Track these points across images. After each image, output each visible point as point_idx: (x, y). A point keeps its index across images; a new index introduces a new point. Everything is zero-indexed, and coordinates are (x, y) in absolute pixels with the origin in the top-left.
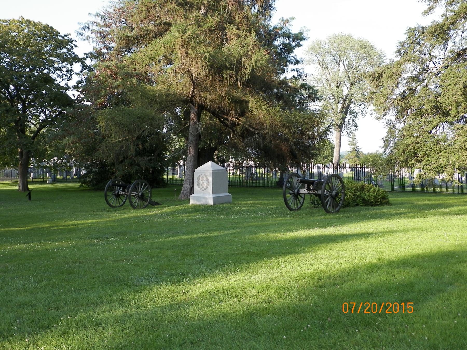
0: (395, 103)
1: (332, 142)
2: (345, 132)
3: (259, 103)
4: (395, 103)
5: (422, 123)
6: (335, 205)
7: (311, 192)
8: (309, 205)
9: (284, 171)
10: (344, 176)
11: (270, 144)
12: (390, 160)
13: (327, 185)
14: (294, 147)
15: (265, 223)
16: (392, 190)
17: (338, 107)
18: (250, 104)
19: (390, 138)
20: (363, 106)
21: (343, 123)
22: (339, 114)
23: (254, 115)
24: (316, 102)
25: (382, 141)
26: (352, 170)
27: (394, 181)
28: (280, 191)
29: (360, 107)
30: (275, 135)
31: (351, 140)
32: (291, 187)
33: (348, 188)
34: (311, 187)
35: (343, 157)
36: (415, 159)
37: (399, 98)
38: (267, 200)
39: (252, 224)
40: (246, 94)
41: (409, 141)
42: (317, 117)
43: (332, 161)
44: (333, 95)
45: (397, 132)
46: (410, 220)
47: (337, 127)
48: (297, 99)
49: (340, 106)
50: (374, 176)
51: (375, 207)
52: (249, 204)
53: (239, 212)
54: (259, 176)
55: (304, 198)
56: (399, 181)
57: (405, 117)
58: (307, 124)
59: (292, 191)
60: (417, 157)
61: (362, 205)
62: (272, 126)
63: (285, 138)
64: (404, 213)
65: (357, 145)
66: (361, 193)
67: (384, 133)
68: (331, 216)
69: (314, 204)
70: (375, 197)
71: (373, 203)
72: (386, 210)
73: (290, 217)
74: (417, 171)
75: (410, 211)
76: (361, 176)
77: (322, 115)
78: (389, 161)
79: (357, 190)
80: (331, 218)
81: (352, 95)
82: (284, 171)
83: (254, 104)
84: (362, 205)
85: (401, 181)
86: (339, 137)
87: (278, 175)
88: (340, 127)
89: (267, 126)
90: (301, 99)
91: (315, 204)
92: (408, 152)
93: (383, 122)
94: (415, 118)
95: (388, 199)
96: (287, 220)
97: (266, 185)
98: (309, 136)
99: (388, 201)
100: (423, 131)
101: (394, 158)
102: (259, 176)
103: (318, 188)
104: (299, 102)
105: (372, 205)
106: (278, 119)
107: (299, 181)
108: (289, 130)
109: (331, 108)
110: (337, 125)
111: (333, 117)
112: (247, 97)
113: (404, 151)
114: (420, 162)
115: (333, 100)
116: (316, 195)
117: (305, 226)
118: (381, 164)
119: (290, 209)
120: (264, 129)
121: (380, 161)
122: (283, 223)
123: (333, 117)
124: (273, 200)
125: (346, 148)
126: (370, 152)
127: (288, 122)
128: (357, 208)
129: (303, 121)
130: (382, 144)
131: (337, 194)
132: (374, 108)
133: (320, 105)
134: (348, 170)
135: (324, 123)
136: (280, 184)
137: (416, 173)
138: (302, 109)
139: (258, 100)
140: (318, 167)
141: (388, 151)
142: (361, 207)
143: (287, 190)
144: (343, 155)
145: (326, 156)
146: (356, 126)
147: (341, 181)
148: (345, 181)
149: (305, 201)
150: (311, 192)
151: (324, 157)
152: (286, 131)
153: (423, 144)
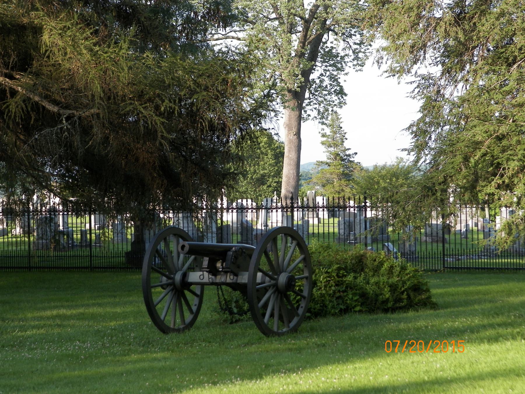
0: (441, 30)
1: (276, 138)
2: (311, 111)
3: (69, 33)
4: (441, 30)
5: (512, 84)
6: (287, 313)
7: (220, 279)
8: (216, 316)
9: (145, 220)
10: (311, 230)
11: (106, 148)
12: (430, 185)
13: (263, 258)
14: (171, 156)
15: (91, 371)
16: (439, 266)
17: (290, 42)
18: (46, 37)
19: (431, 124)
20: (357, 38)
21: (307, 83)
22: (293, 61)
23: (57, 66)
24: (228, 29)
25: (407, 133)
26: (332, 213)
27: (444, 241)
28: (137, 278)
29: (351, 41)
30: (116, 122)
31: (328, 131)
32: (164, 266)
33: (320, 264)
34: (219, 265)
35: (309, 179)
36: (497, 180)
37: (449, 17)
38: (100, 305)
39: (56, 376)
40: (34, 8)
41: (479, 133)
42: (233, 70)
43: (278, 189)
44: (276, 8)
45: (446, 109)
46: (485, 346)
47: (288, 96)
48: (177, 21)
49: (296, 39)
50: (390, 229)
51: (395, 316)
52: (48, 318)
53: (21, 343)
54: (77, 236)
55: (200, 297)
56: (458, 241)
57: (468, 66)
58: (206, 89)
59: (168, 278)
60: (502, 176)
61: (360, 311)
62: (110, 96)
63: (146, 128)
64: (473, 330)
65: (346, 144)
66: (355, 278)
67: (412, 110)
68: (275, 344)
69: (230, 313)
70: (393, 288)
71: (390, 305)
72: (422, 319)
73: (163, 350)
74: (504, 215)
75: (486, 322)
76: (357, 232)
77: (245, 65)
78: (429, 189)
79: (345, 269)
80: (278, 350)
81: (326, 7)
82: (145, 220)
83: (57, 37)
84: (360, 311)
85: (464, 241)
86: (294, 124)
87: (130, 233)
88: (298, 96)
89: (93, 96)
90: (188, 20)
91: (231, 313)
92: (477, 163)
93: (407, 84)
94: (494, 71)
95: (428, 290)
96: (155, 359)
97: (96, 262)
98: (211, 121)
99: (429, 297)
100: (514, 106)
101: (441, 179)
102: (77, 236)
103: (239, 267)
104: (184, 28)
105: (386, 311)
106: (125, 76)
107: (187, 248)
108: (157, 108)
109: (271, 44)
110: (290, 91)
111: (276, 69)
112: (37, 17)
113: (466, 159)
114: (509, 187)
115: (277, 23)
116: (235, 286)
117: (205, 375)
118: (409, 197)
119: (164, 329)
120: (87, 107)
121: (405, 189)
122: (143, 370)
123: (276, 69)
124: (115, 305)
125: (314, 152)
126: (381, 163)
127: (151, 86)
128: (347, 320)
129: (195, 82)
130: (408, 141)
131: (291, 282)
132: (385, 43)
133: (241, 35)
134: (323, 214)
135: (251, 86)
136: (134, 259)
137: (503, 217)
138: (192, 48)
139: (68, 24)
140: (241, 209)
141: (426, 159)
142: (358, 316)
143: (154, 275)
144: (307, 174)
145: (263, 176)
146: (341, 92)
147: (302, 246)
148: (313, 245)
149: (204, 306)
150: (220, 279)
151: (258, 180)
152: (148, 112)
153: (515, 139)
